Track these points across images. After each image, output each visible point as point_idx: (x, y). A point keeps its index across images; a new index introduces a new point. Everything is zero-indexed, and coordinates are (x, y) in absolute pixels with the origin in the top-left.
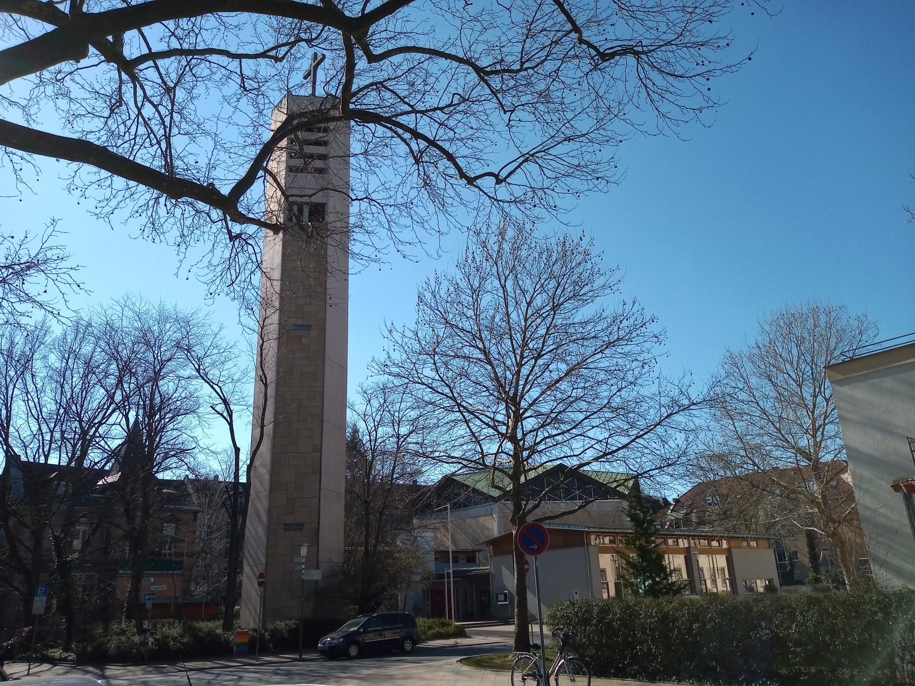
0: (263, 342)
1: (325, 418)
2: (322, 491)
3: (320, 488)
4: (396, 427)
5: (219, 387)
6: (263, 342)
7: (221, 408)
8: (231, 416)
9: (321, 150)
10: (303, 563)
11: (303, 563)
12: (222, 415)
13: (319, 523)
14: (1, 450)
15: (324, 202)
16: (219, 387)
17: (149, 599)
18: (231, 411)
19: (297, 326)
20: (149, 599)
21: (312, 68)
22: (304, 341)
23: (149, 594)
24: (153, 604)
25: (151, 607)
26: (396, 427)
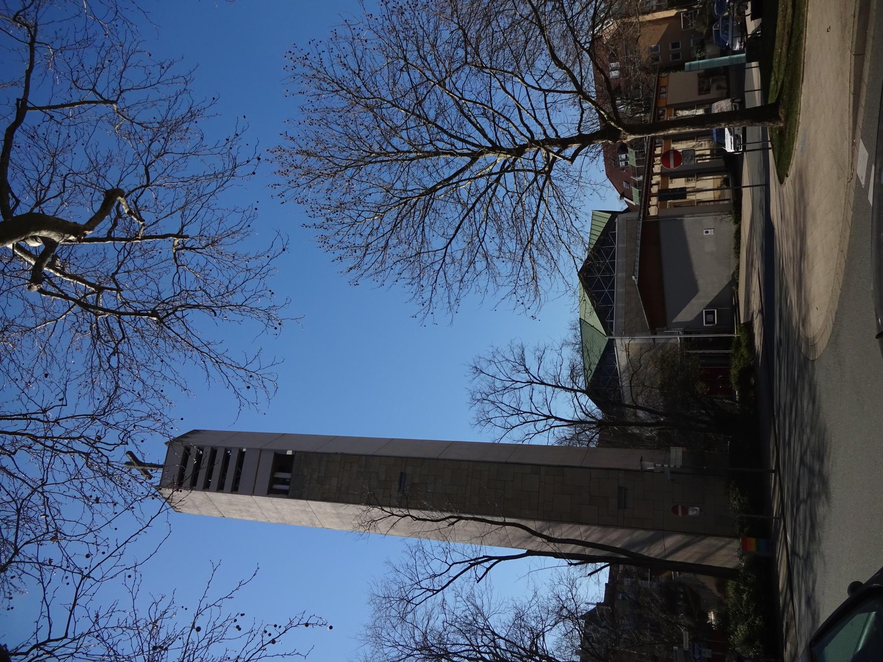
0: (409, 515)
1: (503, 460)
2: (583, 465)
3: (581, 467)
4: (519, 385)
5: (453, 564)
6: (409, 515)
7: (480, 570)
8: (491, 558)
9: (220, 457)
10: (663, 466)
11: (663, 466)
12: (488, 569)
13: (619, 470)
14: (48, 660)
15: (272, 455)
16: (453, 564)
17: (700, 654)
18: (484, 557)
19: (400, 488)
20: (700, 654)
21: (140, 468)
22: (416, 481)
23: (694, 653)
24: (686, 198)
25: (710, 651)
26: (519, 385)
